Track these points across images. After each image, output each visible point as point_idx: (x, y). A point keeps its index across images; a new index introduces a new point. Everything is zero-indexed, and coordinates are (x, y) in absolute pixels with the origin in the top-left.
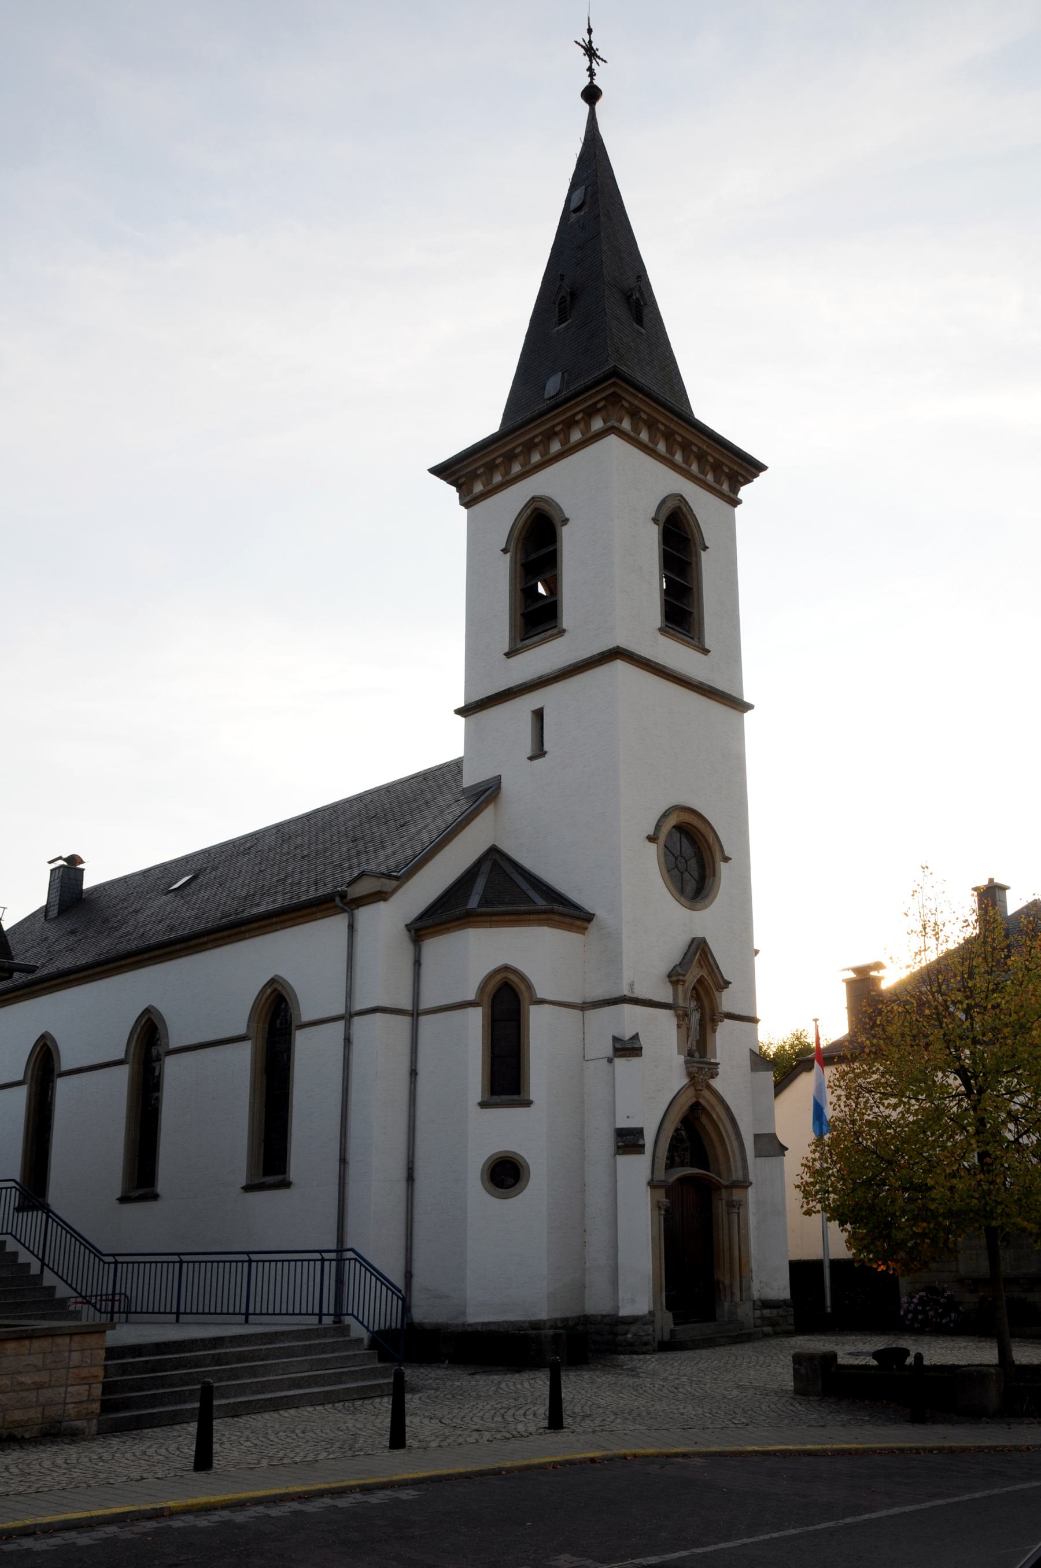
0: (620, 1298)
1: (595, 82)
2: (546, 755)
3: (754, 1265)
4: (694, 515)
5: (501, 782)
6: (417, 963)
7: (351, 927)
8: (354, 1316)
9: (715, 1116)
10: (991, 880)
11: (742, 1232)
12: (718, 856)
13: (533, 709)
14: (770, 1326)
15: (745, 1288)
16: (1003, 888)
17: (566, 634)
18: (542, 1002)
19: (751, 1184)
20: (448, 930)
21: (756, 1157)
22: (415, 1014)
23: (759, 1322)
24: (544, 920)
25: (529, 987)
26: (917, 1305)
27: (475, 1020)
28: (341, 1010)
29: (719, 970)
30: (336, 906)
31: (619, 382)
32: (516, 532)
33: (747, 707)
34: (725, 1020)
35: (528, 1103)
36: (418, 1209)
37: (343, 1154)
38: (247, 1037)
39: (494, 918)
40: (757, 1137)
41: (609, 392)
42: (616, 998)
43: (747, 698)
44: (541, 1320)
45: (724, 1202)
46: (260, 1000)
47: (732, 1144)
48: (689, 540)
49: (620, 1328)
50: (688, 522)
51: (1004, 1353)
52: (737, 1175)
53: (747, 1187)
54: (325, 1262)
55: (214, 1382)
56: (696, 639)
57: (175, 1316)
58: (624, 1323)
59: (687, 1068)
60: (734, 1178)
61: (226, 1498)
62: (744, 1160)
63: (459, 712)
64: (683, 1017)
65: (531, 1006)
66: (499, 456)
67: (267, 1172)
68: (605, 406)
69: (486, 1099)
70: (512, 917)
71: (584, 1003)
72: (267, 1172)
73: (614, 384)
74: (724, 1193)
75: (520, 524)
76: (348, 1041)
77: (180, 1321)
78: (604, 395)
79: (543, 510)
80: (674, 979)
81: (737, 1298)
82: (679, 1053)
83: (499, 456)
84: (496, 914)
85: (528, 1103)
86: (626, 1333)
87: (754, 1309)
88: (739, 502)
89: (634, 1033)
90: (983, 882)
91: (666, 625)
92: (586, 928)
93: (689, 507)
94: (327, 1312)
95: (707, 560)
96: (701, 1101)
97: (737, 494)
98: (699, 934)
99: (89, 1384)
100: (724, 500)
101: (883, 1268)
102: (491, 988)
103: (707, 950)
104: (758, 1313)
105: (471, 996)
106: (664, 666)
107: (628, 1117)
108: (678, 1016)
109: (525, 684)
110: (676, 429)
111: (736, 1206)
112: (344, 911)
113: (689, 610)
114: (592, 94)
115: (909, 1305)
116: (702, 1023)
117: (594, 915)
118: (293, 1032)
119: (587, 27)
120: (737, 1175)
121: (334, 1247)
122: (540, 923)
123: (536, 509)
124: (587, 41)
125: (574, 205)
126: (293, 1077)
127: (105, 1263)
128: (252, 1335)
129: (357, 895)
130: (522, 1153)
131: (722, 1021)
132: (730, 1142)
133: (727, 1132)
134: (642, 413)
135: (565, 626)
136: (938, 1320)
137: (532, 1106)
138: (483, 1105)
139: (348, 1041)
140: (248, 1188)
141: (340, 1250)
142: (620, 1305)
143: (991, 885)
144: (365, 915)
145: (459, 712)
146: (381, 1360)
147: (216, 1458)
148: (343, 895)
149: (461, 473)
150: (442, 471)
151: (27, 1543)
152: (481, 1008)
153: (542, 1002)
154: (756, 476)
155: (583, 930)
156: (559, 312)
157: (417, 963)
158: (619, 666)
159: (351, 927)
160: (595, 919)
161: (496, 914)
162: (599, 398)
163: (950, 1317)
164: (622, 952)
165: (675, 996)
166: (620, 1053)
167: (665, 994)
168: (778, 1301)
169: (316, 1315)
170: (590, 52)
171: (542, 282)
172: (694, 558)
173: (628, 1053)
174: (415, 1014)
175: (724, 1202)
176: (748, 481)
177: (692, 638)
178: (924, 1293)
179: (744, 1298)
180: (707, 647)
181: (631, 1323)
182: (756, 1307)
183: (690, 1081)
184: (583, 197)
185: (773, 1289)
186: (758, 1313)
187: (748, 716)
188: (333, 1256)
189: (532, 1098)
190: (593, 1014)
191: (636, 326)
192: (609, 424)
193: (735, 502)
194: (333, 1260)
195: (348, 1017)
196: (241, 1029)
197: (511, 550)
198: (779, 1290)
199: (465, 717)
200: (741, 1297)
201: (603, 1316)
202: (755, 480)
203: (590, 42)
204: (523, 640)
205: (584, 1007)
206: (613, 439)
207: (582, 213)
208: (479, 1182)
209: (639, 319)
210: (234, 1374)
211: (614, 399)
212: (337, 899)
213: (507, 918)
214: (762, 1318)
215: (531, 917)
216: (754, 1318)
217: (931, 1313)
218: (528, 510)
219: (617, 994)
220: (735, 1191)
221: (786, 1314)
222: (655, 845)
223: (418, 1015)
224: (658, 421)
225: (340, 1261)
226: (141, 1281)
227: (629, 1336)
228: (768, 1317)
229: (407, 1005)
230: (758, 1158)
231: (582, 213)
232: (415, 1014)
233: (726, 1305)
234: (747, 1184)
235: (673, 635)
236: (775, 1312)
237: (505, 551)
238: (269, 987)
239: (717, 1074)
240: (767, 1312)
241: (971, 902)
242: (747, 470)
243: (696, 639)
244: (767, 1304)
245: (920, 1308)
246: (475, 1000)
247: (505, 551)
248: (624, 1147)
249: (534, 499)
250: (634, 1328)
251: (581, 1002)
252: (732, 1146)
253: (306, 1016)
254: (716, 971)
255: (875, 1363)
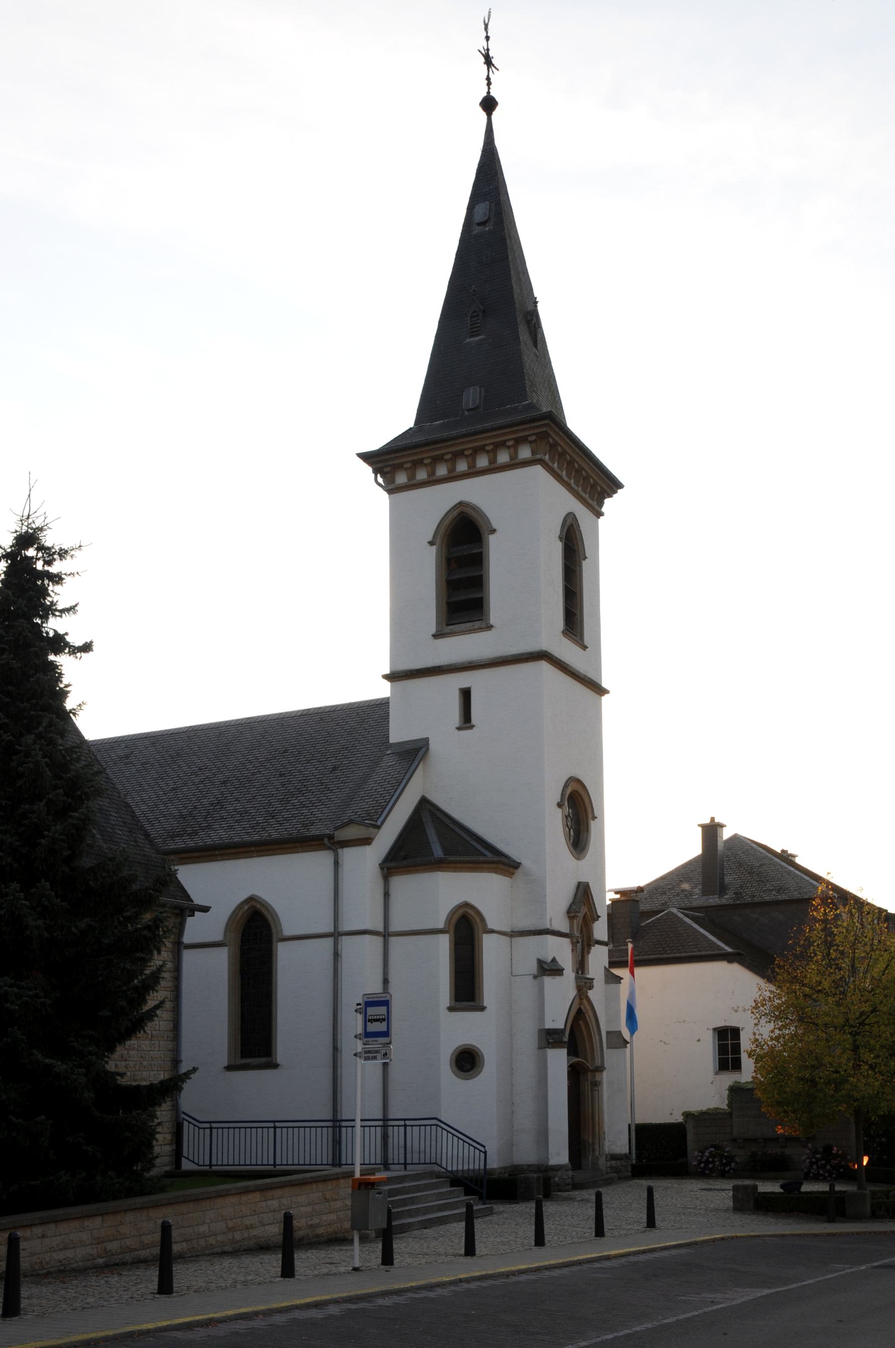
0: (550, 1152)
1: (492, 94)
2: (474, 728)
3: (606, 1129)
4: (580, 531)
5: (428, 744)
6: (387, 895)
7: (336, 863)
8: (438, 1165)
10: (713, 819)
11: (600, 1104)
12: (590, 816)
13: (461, 687)
14: (615, 1172)
15: (601, 1146)
16: (722, 826)
17: (493, 629)
18: (492, 931)
19: (605, 1068)
20: (417, 871)
22: (387, 935)
23: (609, 1170)
24: (493, 868)
25: (483, 919)
26: (708, 1157)
27: (443, 944)
28: (330, 929)
29: (595, 907)
30: (324, 844)
31: (551, 424)
32: (442, 530)
33: (602, 691)
34: (596, 945)
35: (482, 1009)
36: (392, 1087)
38: (224, 944)
39: (458, 865)
40: (608, 1033)
41: (542, 430)
42: (541, 930)
43: (605, 684)
44: (493, 1169)
45: (589, 1082)
46: (237, 914)
47: (596, 1039)
48: (575, 551)
49: (550, 1174)
50: (576, 535)
51: (832, 1187)
52: (598, 1063)
53: (602, 1071)
54: (408, 1127)
55: (393, 1208)
56: (579, 636)
57: (403, 1166)
58: (554, 1170)
59: (577, 982)
60: (596, 1065)
61: (565, 1260)
62: (602, 1051)
63: (386, 677)
64: (574, 944)
65: (484, 935)
66: (428, 458)
67: (244, 1055)
68: (535, 441)
69: (453, 1005)
70: (471, 865)
71: (512, 932)
72: (244, 1055)
73: (547, 425)
74: (589, 1075)
75: (447, 522)
76: (336, 955)
77: (407, 1169)
78: (536, 431)
79: (467, 514)
80: (572, 915)
81: (597, 1153)
83: (428, 458)
84: (460, 862)
85: (482, 1009)
86: (555, 1177)
87: (607, 1161)
88: (602, 514)
90: (707, 821)
91: (566, 629)
92: (513, 874)
93: (578, 524)
94: (280, 1163)
95: (585, 564)
96: (582, 1007)
97: (601, 508)
98: (583, 879)
100: (593, 513)
101: (782, 1131)
102: (455, 919)
104: (609, 1164)
105: (441, 925)
106: (568, 665)
107: (553, 1021)
108: (572, 943)
109: (472, 670)
110: (560, 441)
111: (596, 1084)
112: (329, 848)
113: (573, 610)
114: (489, 104)
115: (702, 1158)
116: (583, 949)
117: (521, 863)
118: (274, 944)
119: (489, 42)
120: (598, 1063)
121: (381, 1117)
122: (490, 870)
123: (462, 513)
124: (486, 48)
125: (478, 217)
126: (276, 982)
127: (199, 1128)
128: (394, 1177)
129: (343, 839)
130: (479, 1046)
131: (594, 946)
132: (595, 1037)
133: (594, 1031)
134: (567, 455)
135: (492, 622)
136: (722, 1168)
137: (486, 1011)
138: (451, 1009)
139: (336, 955)
140: (229, 1068)
141: (385, 1119)
143: (712, 824)
144: (349, 855)
145: (386, 677)
146: (466, 1194)
147: (177, 1277)
148: (331, 837)
149: (389, 463)
150: (366, 457)
151: (380, 1301)
152: (448, 935)
153: (492, 931)
154: (616, 492)
155: (510, 874)
156: (471, 325)
157: (387, 895)
158: (544, 665)
159: (336, 863)
160: (521, 867)
161: (460, 862)
162: (531, 432)
163: (730, 1166)
164: (546, 895)
165: (571, 927)
166: (548, 973)
167: (565, 928)
168: (622, 1155)
169: (402, 1164)
170: (488, 61)
171: (448, 286)
172: (578, 567)
173: (554, 973)
174: (386, 935)
175: (589, 1082)
176: (610, 496)
177: (576, 636)
178: (713, 1149)
180: (585, 644)
181: (558, 1170)
183: (578, 992)
184: (488, 213)
186: (609, 1164)
187: (605, 699)
188: (381, 1123)
189: (485, 1005)
190: (515, 940)
191: (534, 349)
192: (538, 456)
193: (599, 514)
194: (330, 1127)
195: (336, 935)
196: (218, 937)
197: (438, 544)
199: (390, 682)
200: (599, 1152)
201: (529, 1166)
202: (614, 495)
203: (488, 50)
204: (448, 625)
205: (514, 934)
206: (538, 469)
207: (487, 229)
208: (449, 1067)
209: (535, 344)
210: (404, 1202)
211: (543, 436)
212: (326, 840)
213: (468, 865)
214: (611, 1167)
215: (485, 866)
216: (607, 1167)
217: (717, 1163)
218: (455, 512)
219: (542, 927)
220: (597, 1074)
222: (561, 810)
223: (384, 936)
224: (567, 453)
225: (385, 1127)
226: (242, 1140)
227: (557, 1179)
229: (380, 928)
231: (487, 229)
232: (387, 935)
233: (590, 1157)
234: (602, 1069)
235: (570, 637)
236: (619, 1163)
237: (431, 543)
238: (247, 904)
239: (593, 987)
240: (613, 1162)
241: (698, 834)
242: (609, 486)
243: (579, 636)
244: (614, 1157)
245: (711, 1160)
246: (444, 928)
247: (431, 543)
248: (552, 1043)
249: (461, 504)
250: (559, 1173)
251: (509, 931)
252: (596, 1040)
253: (287, 931)
254: (593, 907)
255: (781, 1190)
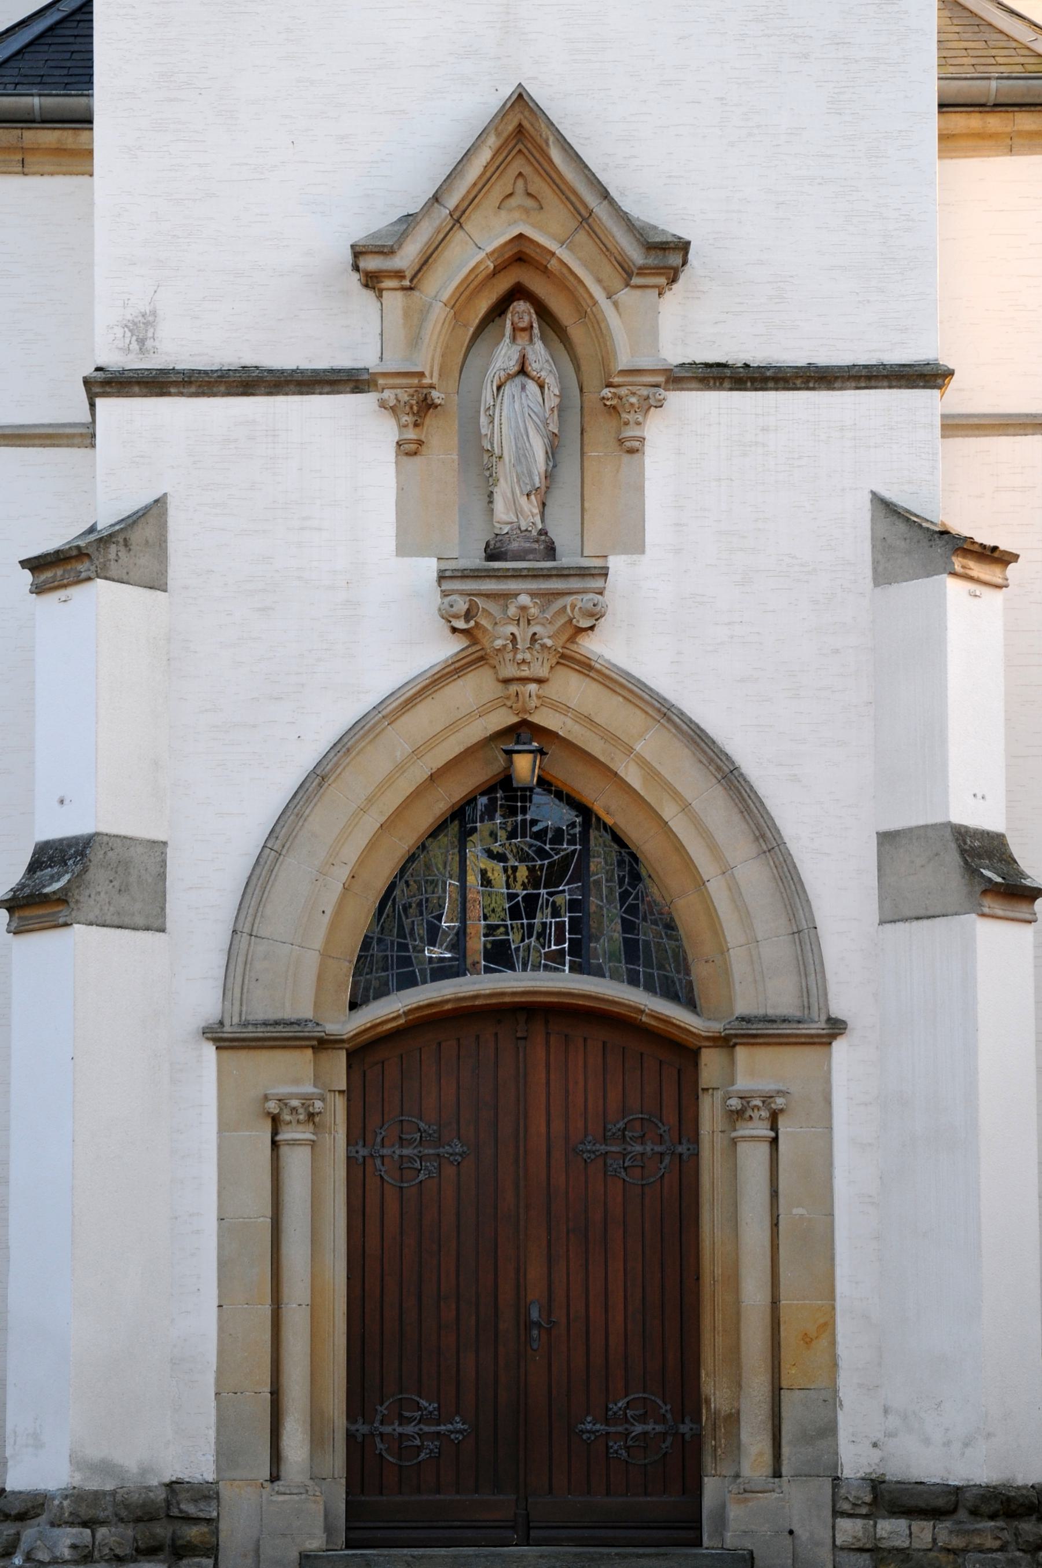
9: (633, 776)
21: (882, 922)
37: (774, 1155)
82: (404, 549)
87: (837, 1513)
89: (145, 498)
99: (781, 1389)
103: (545, 131)
104: (850, 1529)
132: (726, 870)
142: (7, 1455)
179: (785, 1470)
182: (846, 1507)
185: (927, 1441)
186: (850, 1529)
198: (947, 1444)
221: (957, 1542)
228: (899, 1550)
230: (888, 926)
236: (924, 1532)
252: (734, 889)
